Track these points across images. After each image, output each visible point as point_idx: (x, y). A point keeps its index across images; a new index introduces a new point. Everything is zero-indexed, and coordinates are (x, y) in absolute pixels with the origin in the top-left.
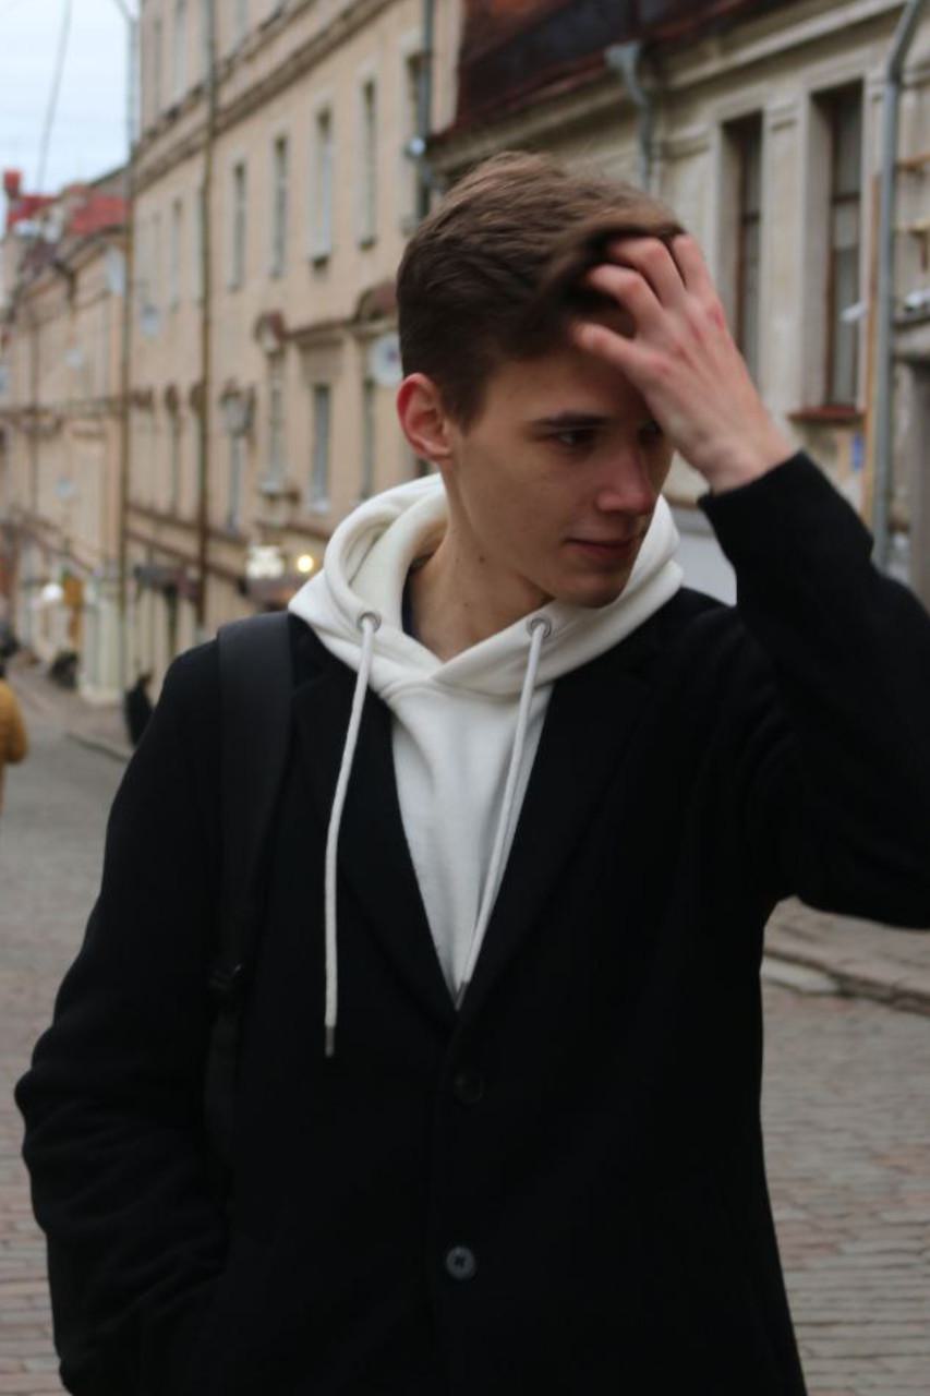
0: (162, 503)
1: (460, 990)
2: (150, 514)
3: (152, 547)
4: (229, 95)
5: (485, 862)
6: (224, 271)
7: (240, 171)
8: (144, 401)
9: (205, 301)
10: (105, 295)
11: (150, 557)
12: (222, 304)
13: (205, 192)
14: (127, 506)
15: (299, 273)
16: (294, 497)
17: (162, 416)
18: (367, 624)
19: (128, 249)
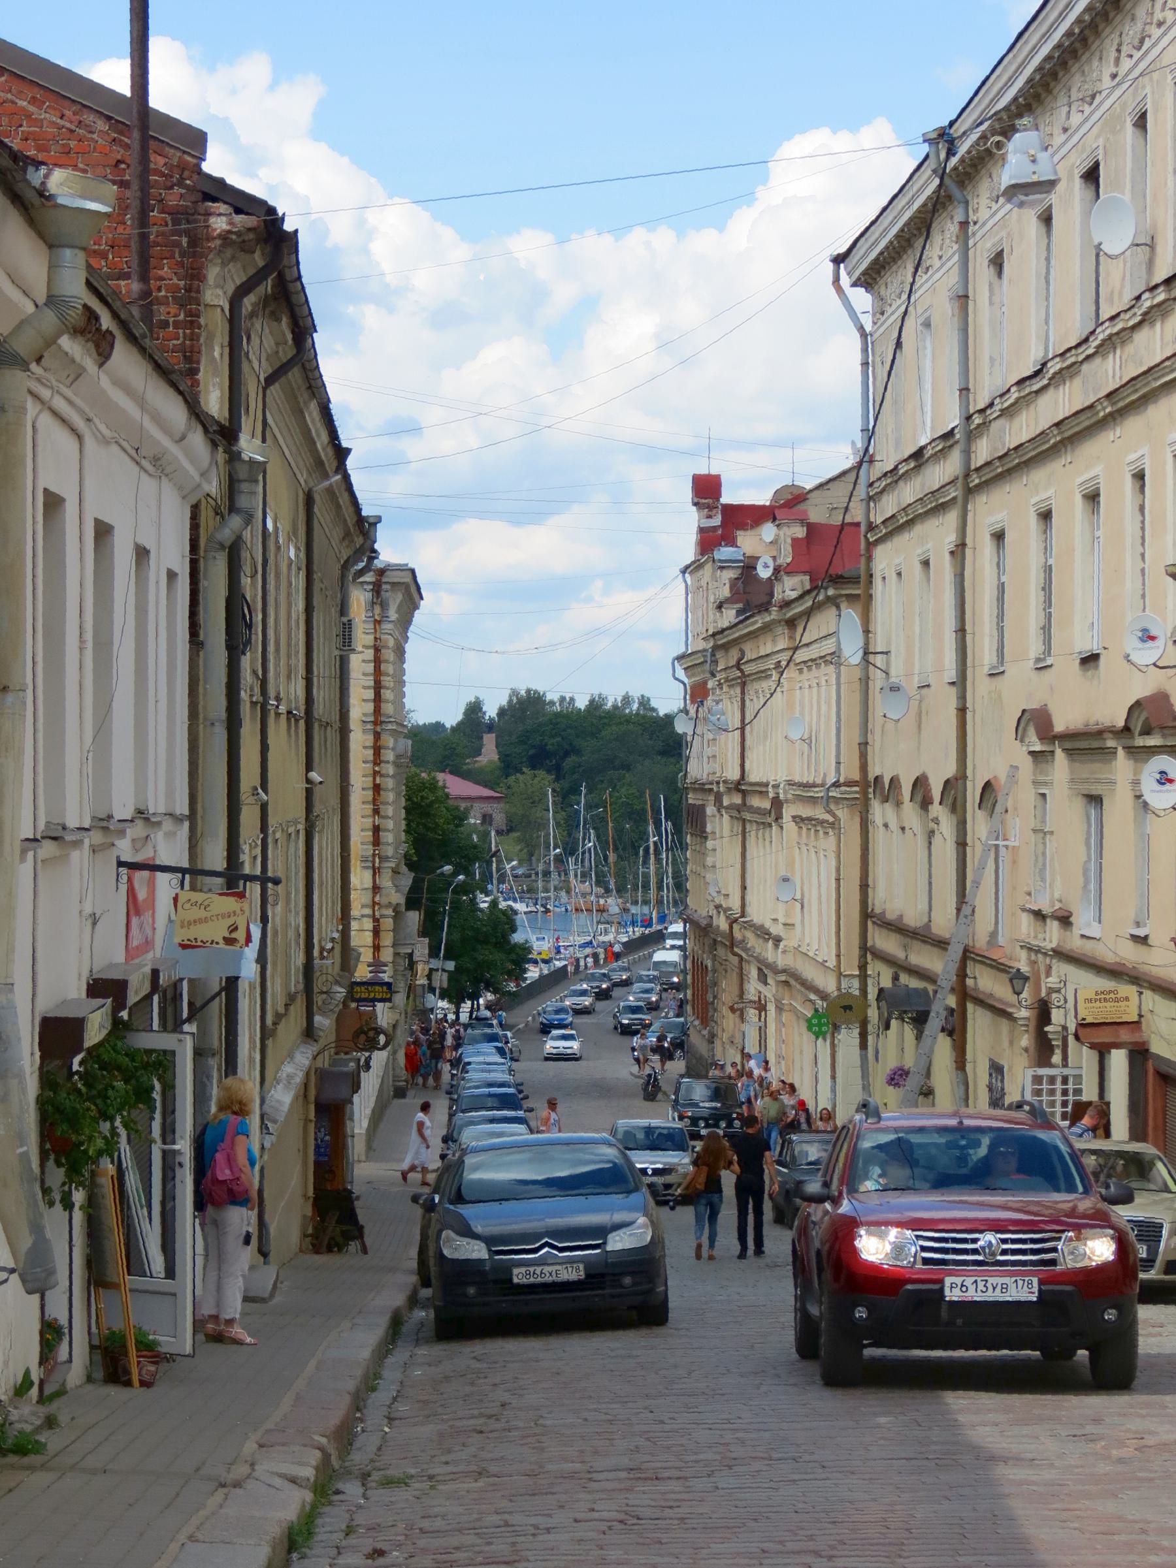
0: (913, 919)
1: (221, 409)
2: (897, 928)
3: (899, 967)
4: (983, 451)
5: (203, 807)
6: (984, 653)
7: (999, 537)
8: (889, 791)
9: (961, 683)
10: (834, 659)
11: (896, 978)
12: (980, 688)
13: (959, 551)
14: (866, 915)
15: (1066, 667)
16: (1065, 920)
17: (910, 810)
18: (541, 1421)
19: (864, 602)
